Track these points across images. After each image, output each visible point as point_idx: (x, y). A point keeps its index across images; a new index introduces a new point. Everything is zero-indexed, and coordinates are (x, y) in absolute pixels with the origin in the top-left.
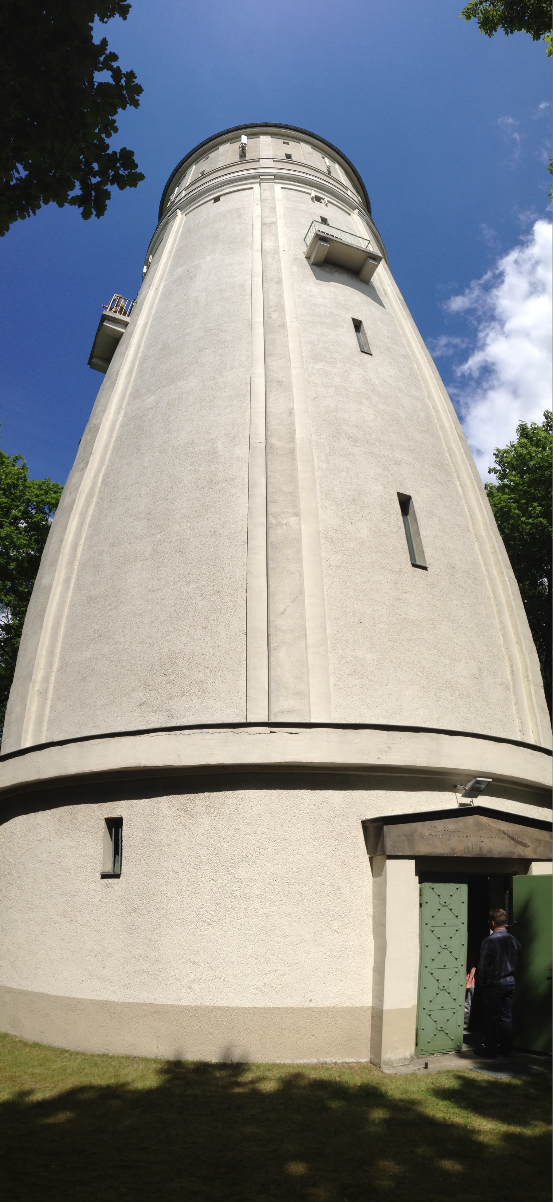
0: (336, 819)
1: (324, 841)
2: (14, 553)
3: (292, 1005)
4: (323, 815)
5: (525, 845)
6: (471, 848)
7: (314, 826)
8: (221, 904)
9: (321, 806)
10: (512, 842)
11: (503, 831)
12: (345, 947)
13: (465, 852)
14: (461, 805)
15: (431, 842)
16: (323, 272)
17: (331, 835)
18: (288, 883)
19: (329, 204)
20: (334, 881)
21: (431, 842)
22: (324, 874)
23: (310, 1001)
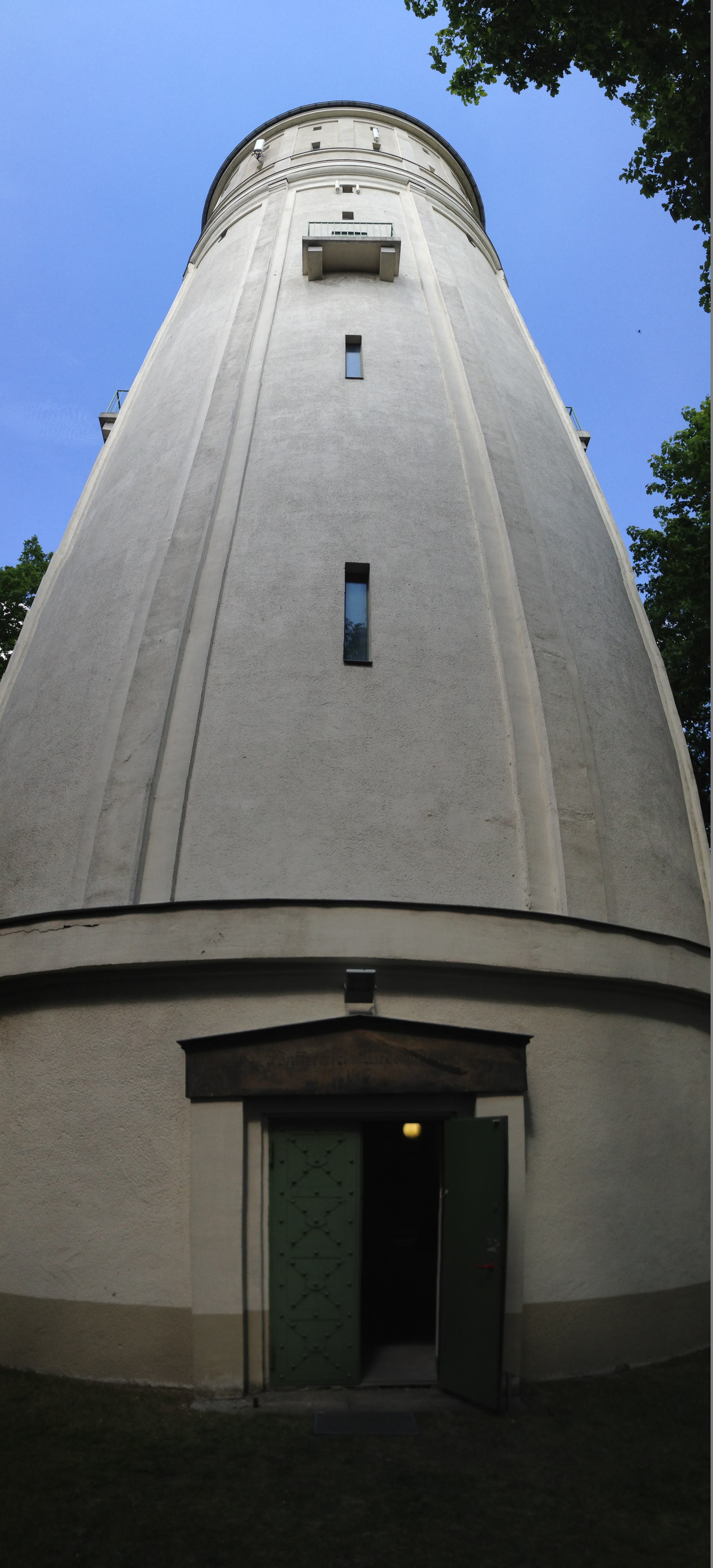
0: (149, 1047)
1: (132, 1081)
2: (674, 481)
7: (120, 1059)
8: (9, 1162)
9: (132, 1029)
14: (351, 1012)
16: (323, 286)
17: (143, 1070)
18: (82, 1138)
19: (363, 190)
22: (128, 1123)
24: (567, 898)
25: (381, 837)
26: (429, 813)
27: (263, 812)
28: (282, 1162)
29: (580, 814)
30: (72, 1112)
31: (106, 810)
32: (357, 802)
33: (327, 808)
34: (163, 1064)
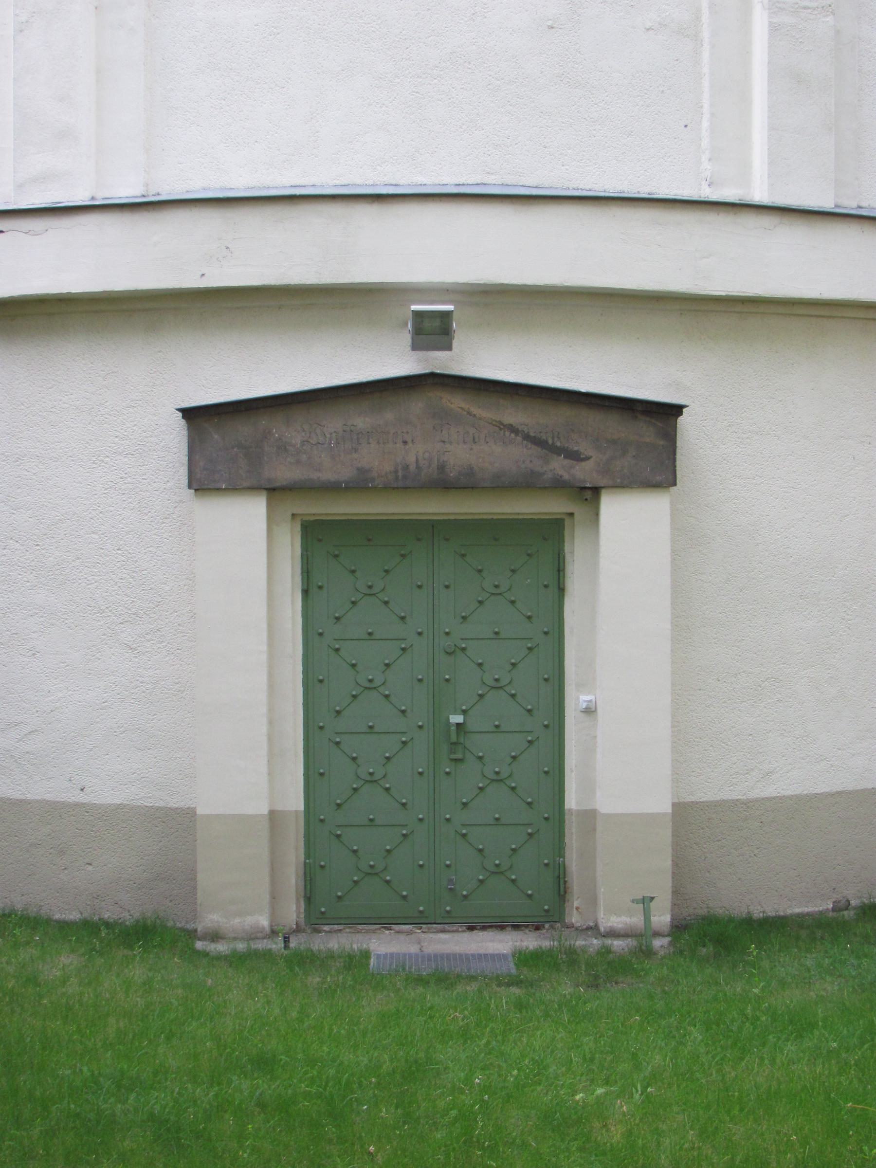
0: (131, 410)
1: (107, 459)
3: (48, 797)
4: (108, 404)
5: (575, 456)
6: (413, 468)
10: (536, 450)
11: (511, 425)
12: (141, 679)
13: (397, 478)
15: (304, 457)
18: (38, 548)
20: (122, 542)
21: (304, 457)
23: (82, 790)
24: (769, 164)
25: (469, 71)
26: (550, 23)
27: (275, 30)
28: (320, 587)
29: (809, 8)
30: (22, 510)
31: (21, 31)
32: (429, 9)
33: (379, 22)
34: (151, 436)
